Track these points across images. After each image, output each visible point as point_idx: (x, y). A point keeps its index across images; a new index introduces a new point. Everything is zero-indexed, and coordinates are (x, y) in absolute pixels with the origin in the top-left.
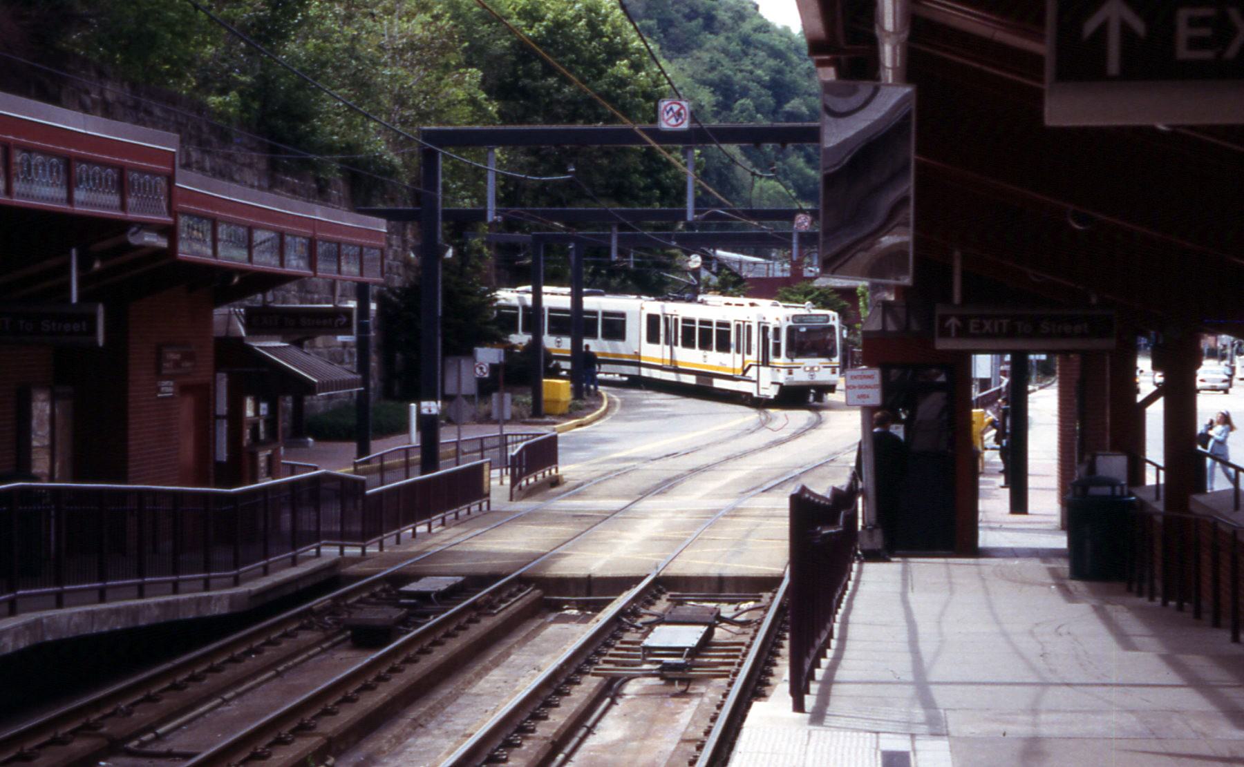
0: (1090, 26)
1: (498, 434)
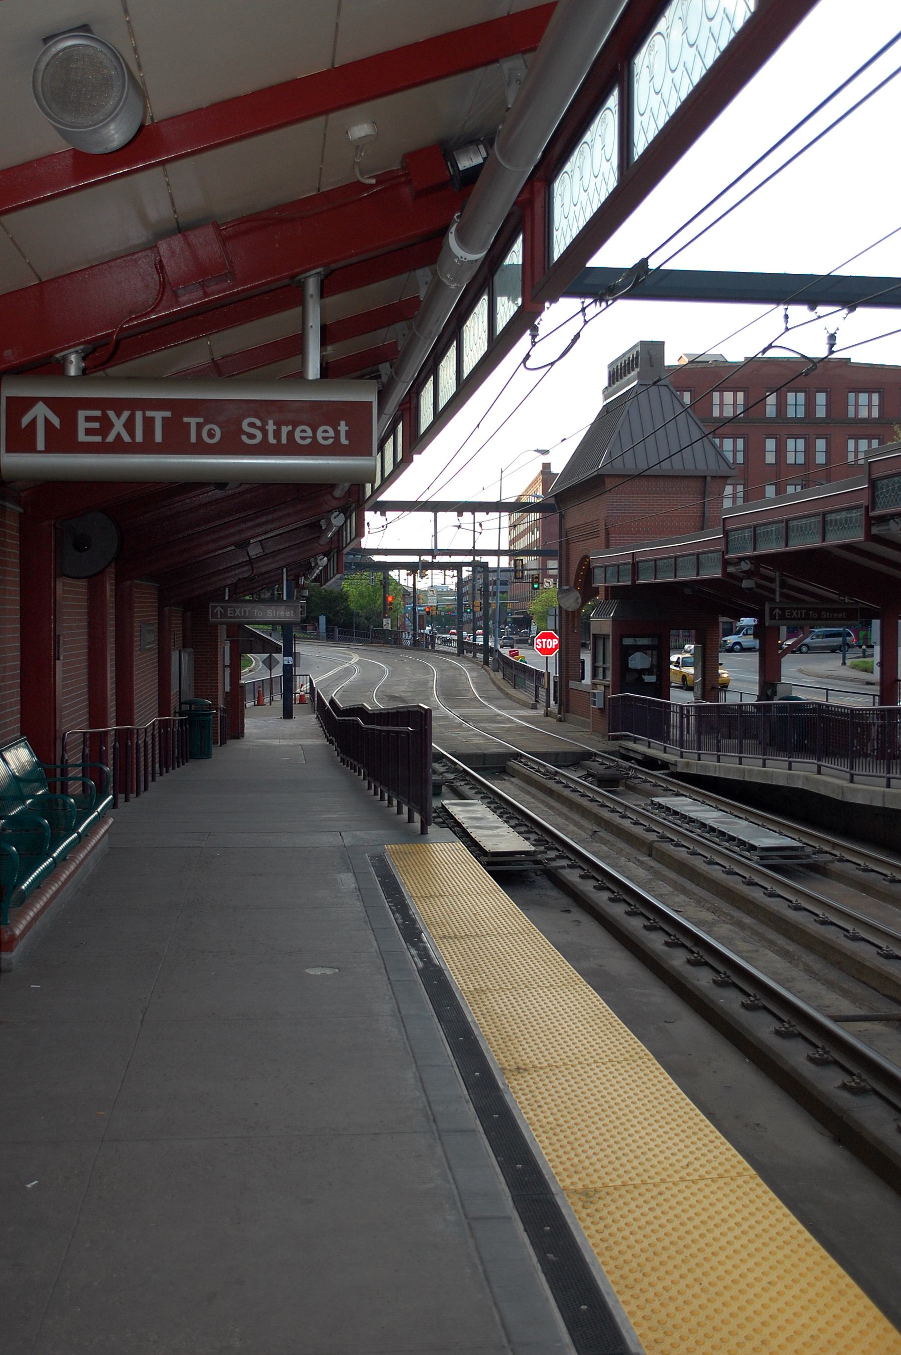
0: (25, 421)
1: (630, 561)
